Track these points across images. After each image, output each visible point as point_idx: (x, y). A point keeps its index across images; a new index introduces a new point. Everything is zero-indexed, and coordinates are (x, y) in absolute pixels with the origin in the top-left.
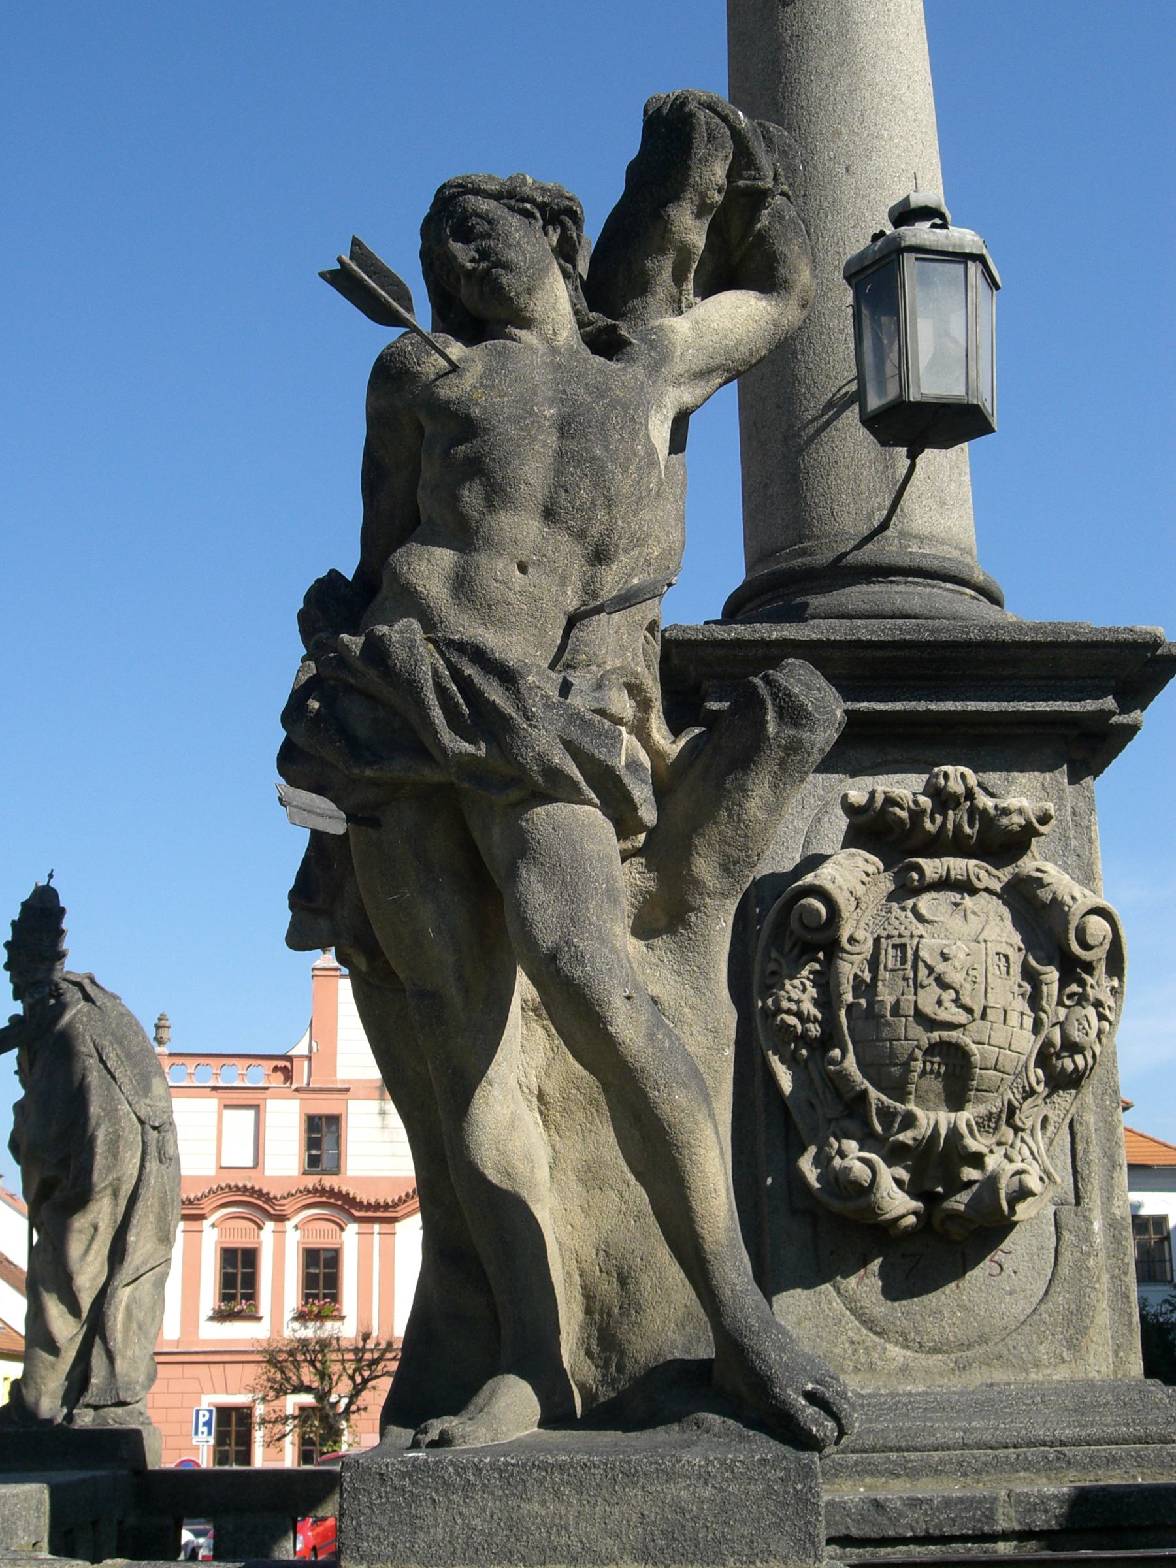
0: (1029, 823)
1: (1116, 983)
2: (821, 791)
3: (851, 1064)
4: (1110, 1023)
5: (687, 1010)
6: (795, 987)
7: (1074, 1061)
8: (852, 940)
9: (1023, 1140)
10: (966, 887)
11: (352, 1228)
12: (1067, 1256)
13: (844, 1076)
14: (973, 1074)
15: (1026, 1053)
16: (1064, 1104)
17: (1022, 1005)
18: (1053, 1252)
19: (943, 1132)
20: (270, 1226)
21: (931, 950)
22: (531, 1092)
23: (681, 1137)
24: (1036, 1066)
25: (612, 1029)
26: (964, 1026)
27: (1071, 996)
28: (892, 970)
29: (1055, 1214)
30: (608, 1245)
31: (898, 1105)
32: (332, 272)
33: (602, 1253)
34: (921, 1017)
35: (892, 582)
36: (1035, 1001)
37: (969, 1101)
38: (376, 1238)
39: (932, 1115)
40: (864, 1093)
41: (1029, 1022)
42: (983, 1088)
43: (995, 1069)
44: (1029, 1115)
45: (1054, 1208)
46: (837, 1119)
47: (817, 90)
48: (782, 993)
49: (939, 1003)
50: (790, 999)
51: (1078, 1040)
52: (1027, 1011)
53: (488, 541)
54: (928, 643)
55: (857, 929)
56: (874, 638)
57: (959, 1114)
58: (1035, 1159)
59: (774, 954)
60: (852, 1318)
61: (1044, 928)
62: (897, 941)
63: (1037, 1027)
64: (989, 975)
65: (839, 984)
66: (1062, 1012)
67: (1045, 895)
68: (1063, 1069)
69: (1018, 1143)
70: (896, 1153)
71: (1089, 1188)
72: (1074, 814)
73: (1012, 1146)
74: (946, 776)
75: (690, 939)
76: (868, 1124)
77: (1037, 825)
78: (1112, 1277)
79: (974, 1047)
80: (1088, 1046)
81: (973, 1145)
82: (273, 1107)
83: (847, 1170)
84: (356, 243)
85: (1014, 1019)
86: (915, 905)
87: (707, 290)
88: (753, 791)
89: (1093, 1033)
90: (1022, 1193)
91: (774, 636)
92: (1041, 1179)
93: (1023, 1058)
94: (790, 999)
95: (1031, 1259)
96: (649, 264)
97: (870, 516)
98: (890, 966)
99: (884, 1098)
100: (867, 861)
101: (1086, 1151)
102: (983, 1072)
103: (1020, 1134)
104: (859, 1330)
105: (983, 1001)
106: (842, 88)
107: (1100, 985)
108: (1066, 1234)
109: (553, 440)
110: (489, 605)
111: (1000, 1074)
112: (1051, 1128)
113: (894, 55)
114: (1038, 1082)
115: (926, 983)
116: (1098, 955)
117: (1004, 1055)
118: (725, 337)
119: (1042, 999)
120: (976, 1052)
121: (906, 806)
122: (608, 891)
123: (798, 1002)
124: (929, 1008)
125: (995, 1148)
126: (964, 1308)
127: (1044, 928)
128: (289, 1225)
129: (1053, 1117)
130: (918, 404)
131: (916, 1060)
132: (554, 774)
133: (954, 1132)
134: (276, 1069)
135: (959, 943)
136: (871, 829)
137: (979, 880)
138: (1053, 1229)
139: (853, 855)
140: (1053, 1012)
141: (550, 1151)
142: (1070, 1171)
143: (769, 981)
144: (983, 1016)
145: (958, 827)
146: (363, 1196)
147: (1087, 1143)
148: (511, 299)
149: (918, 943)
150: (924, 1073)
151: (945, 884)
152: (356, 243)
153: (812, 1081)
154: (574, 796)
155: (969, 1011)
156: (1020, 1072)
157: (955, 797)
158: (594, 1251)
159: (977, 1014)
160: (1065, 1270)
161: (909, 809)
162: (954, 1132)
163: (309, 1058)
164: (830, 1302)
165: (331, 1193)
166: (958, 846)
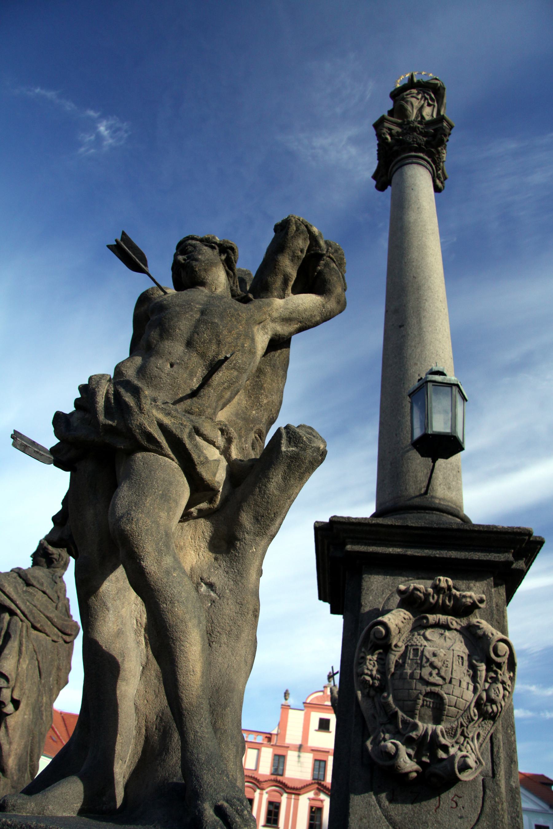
0: (474, 602)
1: (512, 674)
2: (391, 588)
3: (391, 699)
4: (509, 692)
5: (228, 591)
6: (371, 664)
7: (492, 708)
8: (396, 646)
9: (468, 743)
10: (446, 627)
11: (285, 795)
12: (488, 804)
13: (388, 704)
14: (445, 708)
15: (470, 701)
16: (487, 728)
17: (467, 679)
18: (481, 799)
19: (430, 732)
20: (258, 791)
21: (429, 652)
22: (141, 626)
23: (175, 634)
24: (474, 707)
25: (143, 564)
26: (441, 685)
27: (491, 678)
28: (411, 659)
29: (483, 780)
30: (163, 714)
31: (411, 720)
32: (112, 246)
33: (159, 718)
34: (422, 679)
35: (427, 513)
36: (474, 678)
37: (443, 721)
38: (293, 801)
39: (425, 725)
40: (396, 713)
41: (471, 687)
42: (450, 715)
43: (455, 707)
44: (472, 732)
45: (482, 778)
46: (385, 724)
47: (410, 351)
48: (365, 666)
49: (431, 674)
50: (368, 669)
51: (493, 698)
52: (471, 682)
53: (158, 353)
54: (435, 529)
55: (399, 641)
56: (413, 525)
57: (438, 726)
58: (473, 752)
59: (363, 650)
60: (386, 820)
61: (476, 641)
62: (415, 647)
63: (475, 690)
64: (454, 665)
65: (389, 664)
66: (487, 685)
67: (480, 632)
68: (487, 711)
69: (465, 743)
70: (409, 742)
71: (499, 770)
72: (497, 605)
73: (463, 744)
74: (440, 580)
75: (236, 556)
76: (397, 726)
77: (478, 603)
78: (511, 817)
79: (445, 696)
80: (498, 701)
81: (443, 741)
82: (264, 749)
83: (386, 746)
84: (124, 233)
85: (464, 685)
86: (424, 633)
87: (296, 291)
88: (272, 479)
89: (501, 696)
90: (465, 767)
91: (373, 522)
92: (476, 762)
93: (468, 704)
94: (368, 669)
95: (471, 801)
96: (269, 279)
97: (421, 489)
98: (411, 657)
99: (405, 716)
100: (405, 614)
101: (498, 752)
102: (450, 707)
103: (467, 739)
104: (388, 826)
105: (450, 675)
106: (419, 350)
107: (504, 674)
108: (487, 791)
109: (197, 316)
110: (151, 378)
111: (457, 710)
112: (481, 739)
113: (438, 342)
114: (475, 715)
115: (425, 665)
116: (504, 660)
117: (460, 701)
118: (298, 306)
119: (477, 677)
120: (446, 698)
121: (422, 591)
122: (163, 495)
123: (371, 671)
124: (426, 677)
125: (455, 745)
126: (438, 822)
127: (476, 641)
128: (264, 792)
129: (482, 733)
130: (431, 435)
131: (419, 699)
132: (150, 437)
133: (434, 732)
134: (266, 737)
135: (441, 650)
136: (409, 601)
137: (452, 624)
138: (481, 788)
139: (400, 611)
140: (482, 685)
141: (145, 659)
142: (490, 760)
143: (361, 661)
144: (450, 682)
145: (444, 601)
146: (290, 784)
147: (499, 748)
148: (196, 271)
149: (423, 649)
150: (423, 706)
151: (437, 625)
152: (124, 233)
153: (375, 707)
154: (159, 450)
155: (444, 679)
156: (466, 710)
157: (443, 588)
158: (155, 717)
159: (448, 680)
160: (487, 809)
161: (423, 593)
162: (434, 732)
163: (277, 735)
164: (376, 811)
165: (280, 782)
166: (444, 610)
